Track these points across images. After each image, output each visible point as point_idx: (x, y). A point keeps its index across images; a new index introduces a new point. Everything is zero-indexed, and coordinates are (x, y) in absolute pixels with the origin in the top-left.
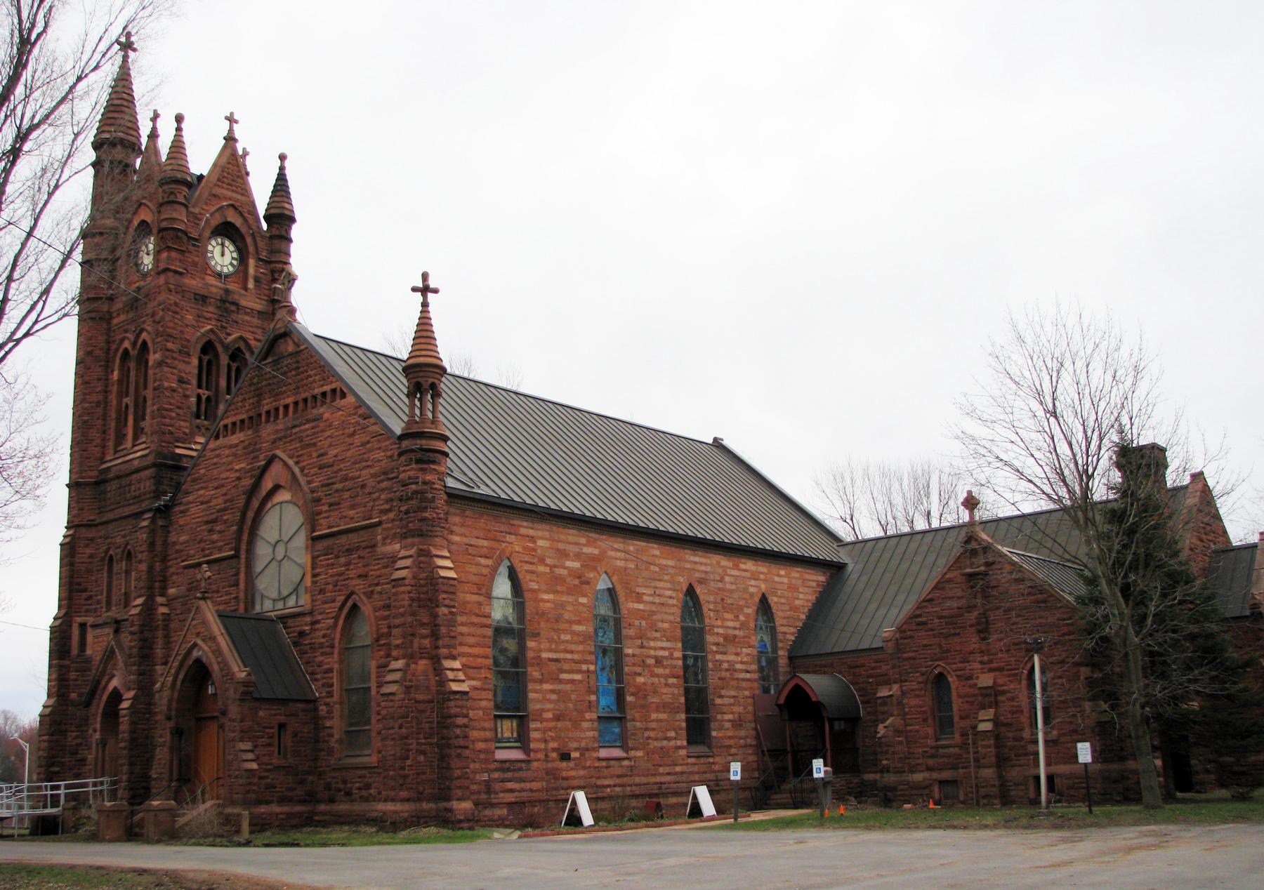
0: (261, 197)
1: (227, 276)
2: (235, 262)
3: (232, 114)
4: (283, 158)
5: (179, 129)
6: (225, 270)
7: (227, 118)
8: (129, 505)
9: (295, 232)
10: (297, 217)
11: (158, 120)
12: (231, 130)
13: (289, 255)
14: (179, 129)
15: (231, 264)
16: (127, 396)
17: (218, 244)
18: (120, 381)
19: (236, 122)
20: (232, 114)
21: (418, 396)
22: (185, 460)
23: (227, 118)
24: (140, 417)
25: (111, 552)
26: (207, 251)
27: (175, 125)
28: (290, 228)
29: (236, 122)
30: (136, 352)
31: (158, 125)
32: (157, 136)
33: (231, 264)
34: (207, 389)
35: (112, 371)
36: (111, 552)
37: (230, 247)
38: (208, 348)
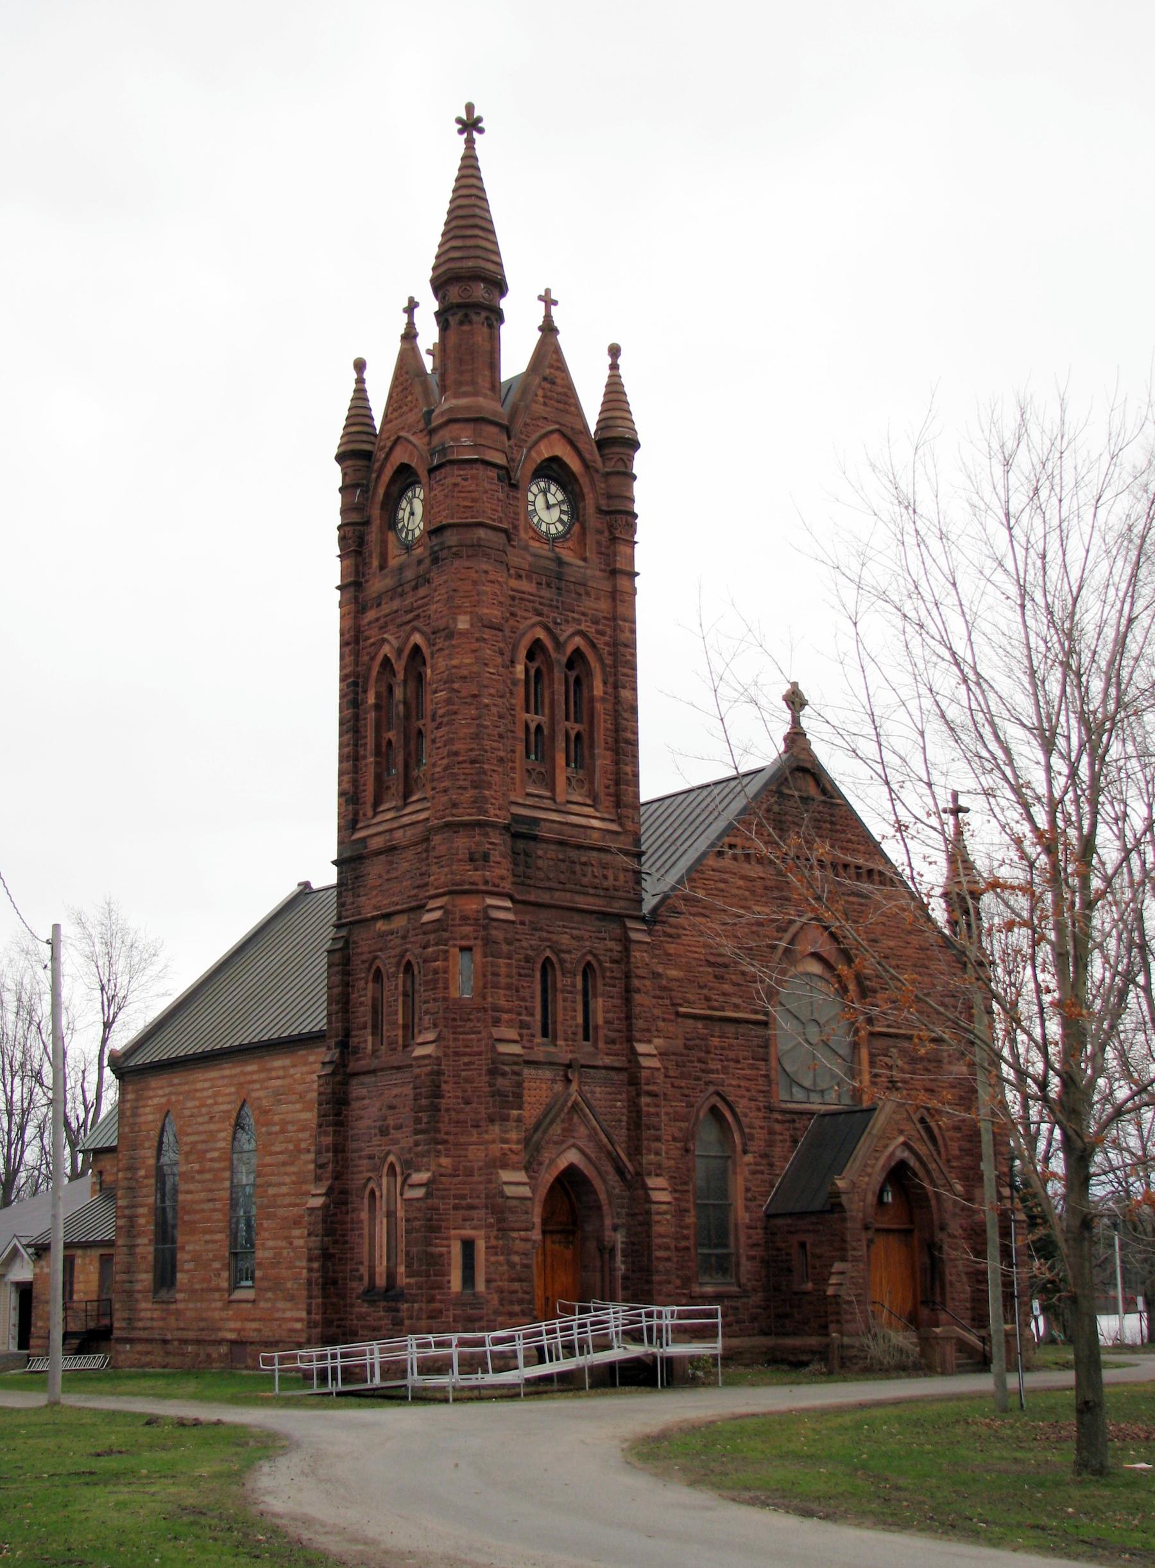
0: (592, 411)
1: (555, 539)
2: (565, 518)
3: (548, 291)
4: (614, 351)
5: (614, 367)
6: (553, 531)
7: (540, 298)
8: (587, 894)
9: (640, 463)
10: (641, 438)
11: (416, 311)
12: (548, 318)
13: (632, 500)
14: (614, 367)
15: (560, 520)
16: (389, 730)
17: (541, 491)
18: (377, 707)
19: (555, 303)
20: (548, 291)
21: (1047, 733)
22: (542, 823)
23: (540, 298)
24: (412, 759)
25: (408, 956)
26: (527, 502)
27: (609, 361)
28: (631, 459)
29: (555, 303)
30: (403, 662)
31: (416, 320)
32: (415, 336)
33: (560, 520)
34: (576, 721)
35: (365, 692)
36: (408, 956)
37: (556, 495)
38: (535, 650)
